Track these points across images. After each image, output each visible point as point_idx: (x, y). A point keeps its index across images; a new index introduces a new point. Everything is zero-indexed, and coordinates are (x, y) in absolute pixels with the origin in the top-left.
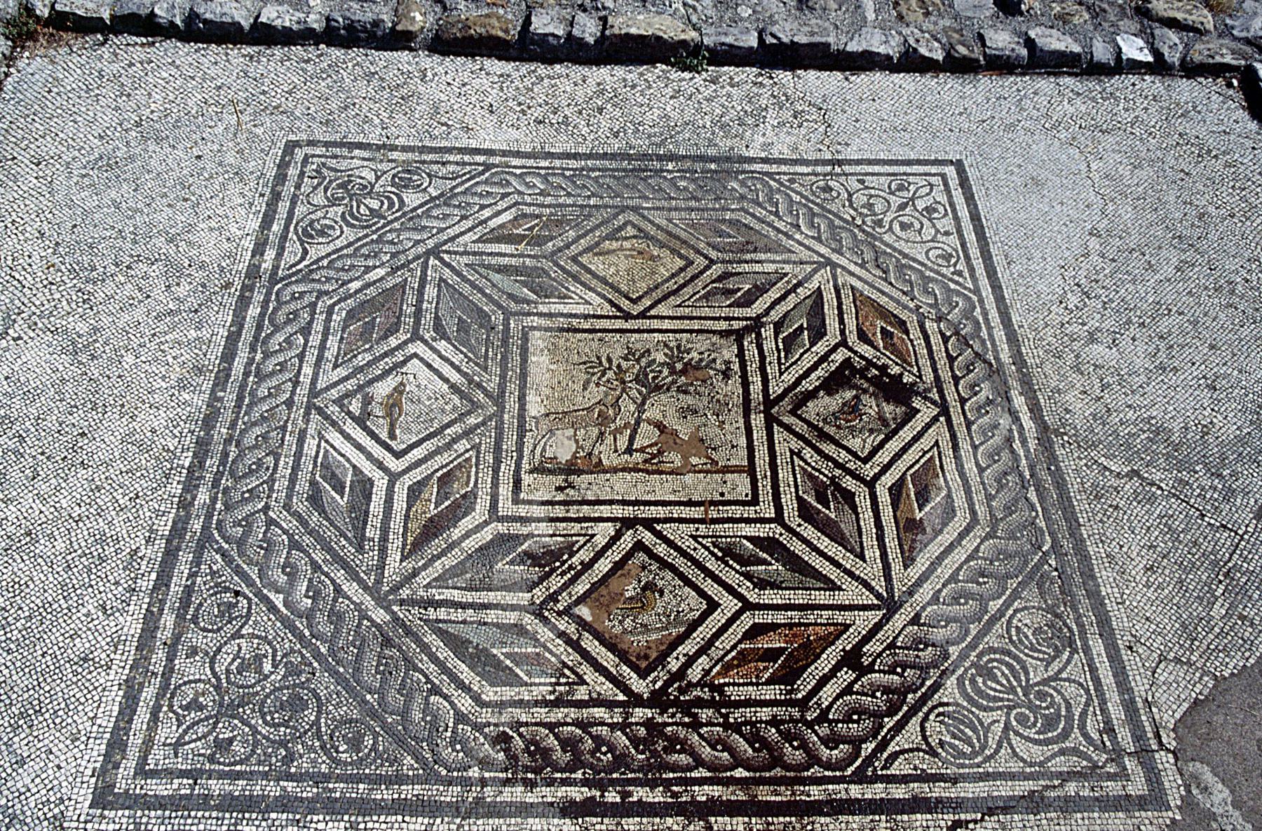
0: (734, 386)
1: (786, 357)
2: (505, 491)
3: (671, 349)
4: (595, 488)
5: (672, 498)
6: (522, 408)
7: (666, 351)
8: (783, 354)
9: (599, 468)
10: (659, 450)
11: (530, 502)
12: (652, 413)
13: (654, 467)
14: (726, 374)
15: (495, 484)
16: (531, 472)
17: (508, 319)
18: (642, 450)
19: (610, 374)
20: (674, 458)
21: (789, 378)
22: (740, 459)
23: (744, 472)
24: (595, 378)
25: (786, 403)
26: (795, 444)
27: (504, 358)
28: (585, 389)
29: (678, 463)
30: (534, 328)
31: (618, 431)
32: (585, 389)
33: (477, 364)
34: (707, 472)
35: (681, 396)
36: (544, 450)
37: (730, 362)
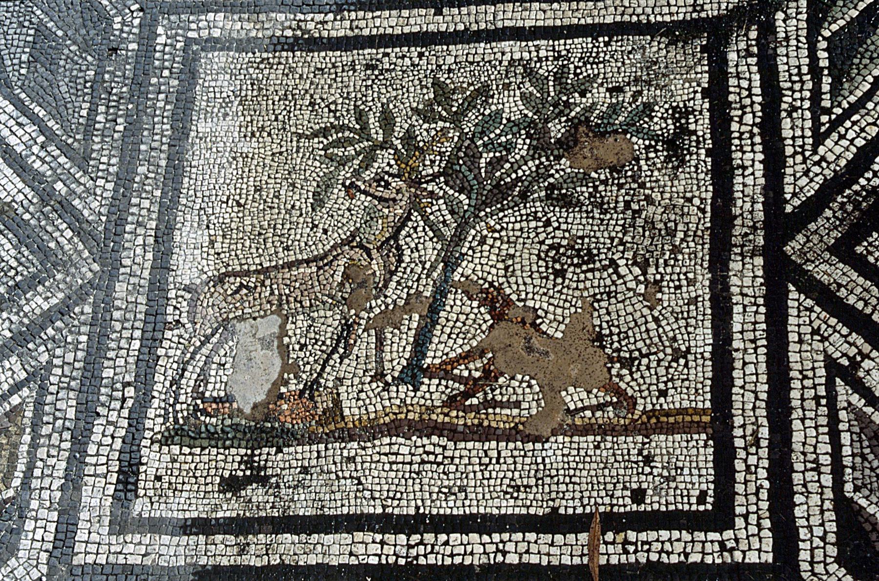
0: (695, 181)
1: (835, 90)
2: (97, 495)
3: (539, 82)
4: (316, 482)
5: (508, 507)
6: (162, 264)
7: (529, 88)
8: (827, 81)
9: (333, 427)
10: (486, 372)
11: (155, 526)
12: (478, 265)
13: (471, 419)
14: (675, 147)
15: (73, 482)
16: (166, 440)
17: (155, 23)
18: (444, 371)
19: (385, 160)
20: (521, 393)
21: (838, 151)
22: (692, 393)
23: (700, 427)
24: (345, 173)
25: (826, 227)
26: (843, 343)
27: (133, 130)
28: (318, 201)
29: (531, 407)
30: (212, 44)
31: (390, 318)
32: (318, 201)
33: (66, 150)
34: (606, 430)
35: (556, 214)
36: (203, 378)
37: (687, 112)
